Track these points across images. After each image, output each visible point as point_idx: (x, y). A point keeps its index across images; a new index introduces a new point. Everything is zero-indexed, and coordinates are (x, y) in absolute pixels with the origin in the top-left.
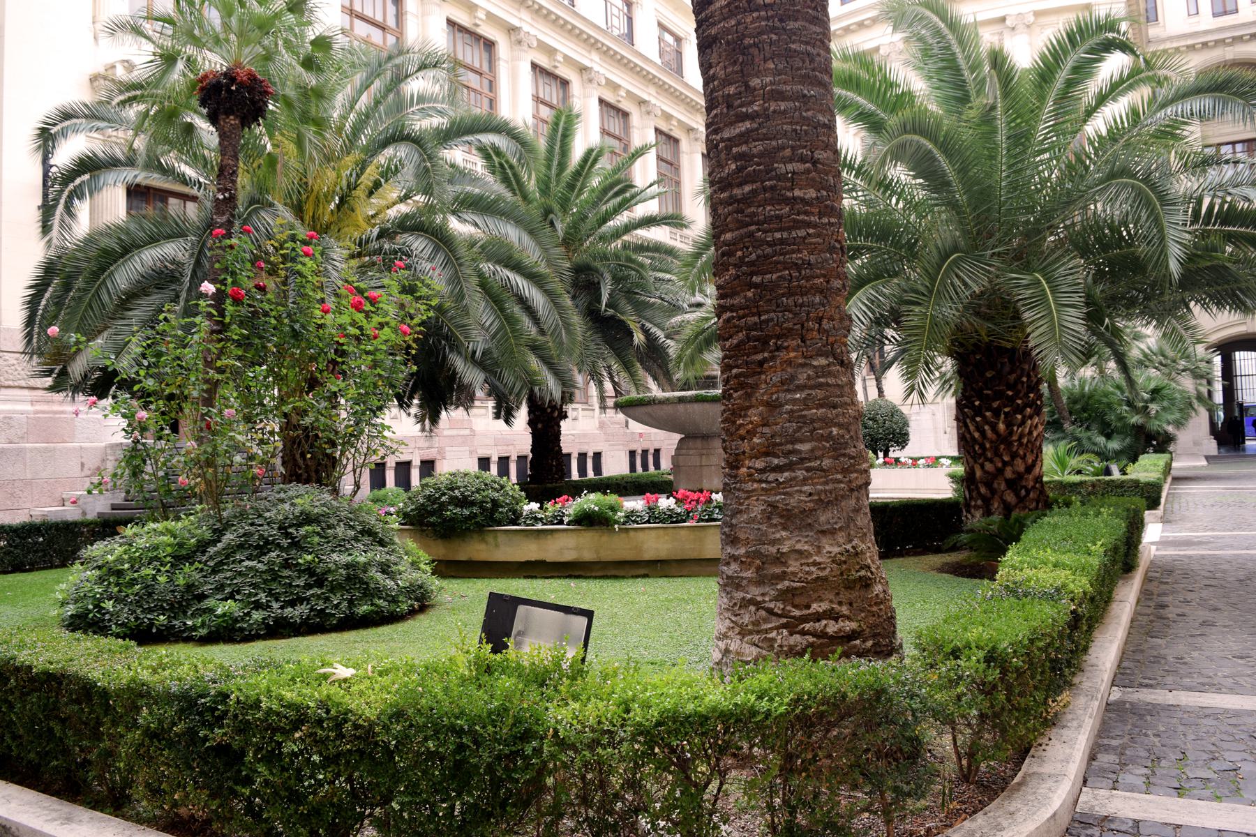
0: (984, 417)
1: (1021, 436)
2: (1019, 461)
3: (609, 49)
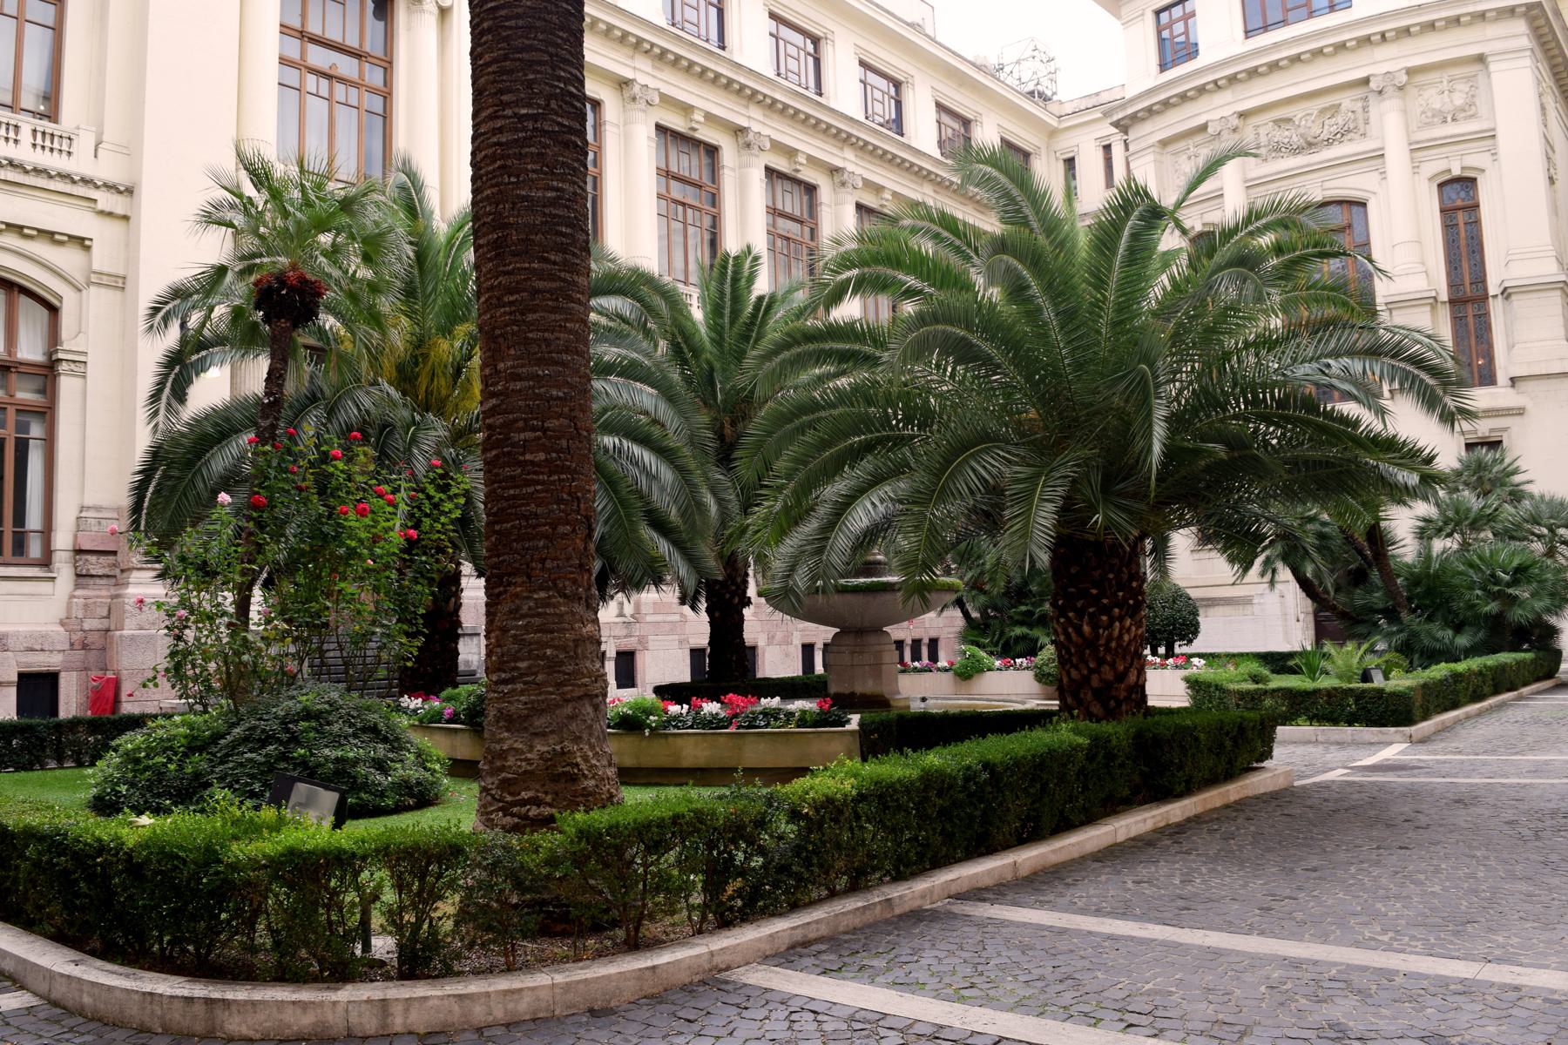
0: (1068, 618)
1: (1110, 639)
2: (1106, 668)
3: (866, 143)
